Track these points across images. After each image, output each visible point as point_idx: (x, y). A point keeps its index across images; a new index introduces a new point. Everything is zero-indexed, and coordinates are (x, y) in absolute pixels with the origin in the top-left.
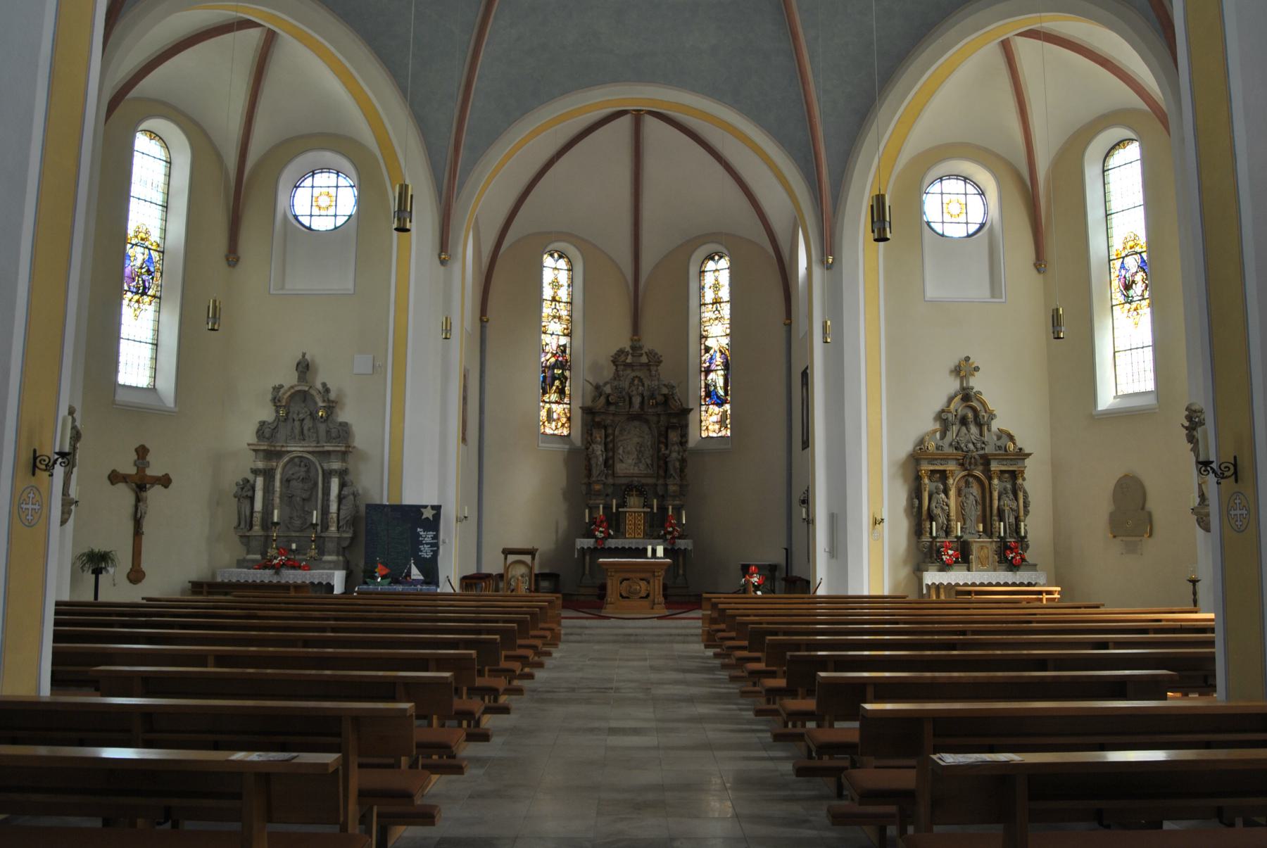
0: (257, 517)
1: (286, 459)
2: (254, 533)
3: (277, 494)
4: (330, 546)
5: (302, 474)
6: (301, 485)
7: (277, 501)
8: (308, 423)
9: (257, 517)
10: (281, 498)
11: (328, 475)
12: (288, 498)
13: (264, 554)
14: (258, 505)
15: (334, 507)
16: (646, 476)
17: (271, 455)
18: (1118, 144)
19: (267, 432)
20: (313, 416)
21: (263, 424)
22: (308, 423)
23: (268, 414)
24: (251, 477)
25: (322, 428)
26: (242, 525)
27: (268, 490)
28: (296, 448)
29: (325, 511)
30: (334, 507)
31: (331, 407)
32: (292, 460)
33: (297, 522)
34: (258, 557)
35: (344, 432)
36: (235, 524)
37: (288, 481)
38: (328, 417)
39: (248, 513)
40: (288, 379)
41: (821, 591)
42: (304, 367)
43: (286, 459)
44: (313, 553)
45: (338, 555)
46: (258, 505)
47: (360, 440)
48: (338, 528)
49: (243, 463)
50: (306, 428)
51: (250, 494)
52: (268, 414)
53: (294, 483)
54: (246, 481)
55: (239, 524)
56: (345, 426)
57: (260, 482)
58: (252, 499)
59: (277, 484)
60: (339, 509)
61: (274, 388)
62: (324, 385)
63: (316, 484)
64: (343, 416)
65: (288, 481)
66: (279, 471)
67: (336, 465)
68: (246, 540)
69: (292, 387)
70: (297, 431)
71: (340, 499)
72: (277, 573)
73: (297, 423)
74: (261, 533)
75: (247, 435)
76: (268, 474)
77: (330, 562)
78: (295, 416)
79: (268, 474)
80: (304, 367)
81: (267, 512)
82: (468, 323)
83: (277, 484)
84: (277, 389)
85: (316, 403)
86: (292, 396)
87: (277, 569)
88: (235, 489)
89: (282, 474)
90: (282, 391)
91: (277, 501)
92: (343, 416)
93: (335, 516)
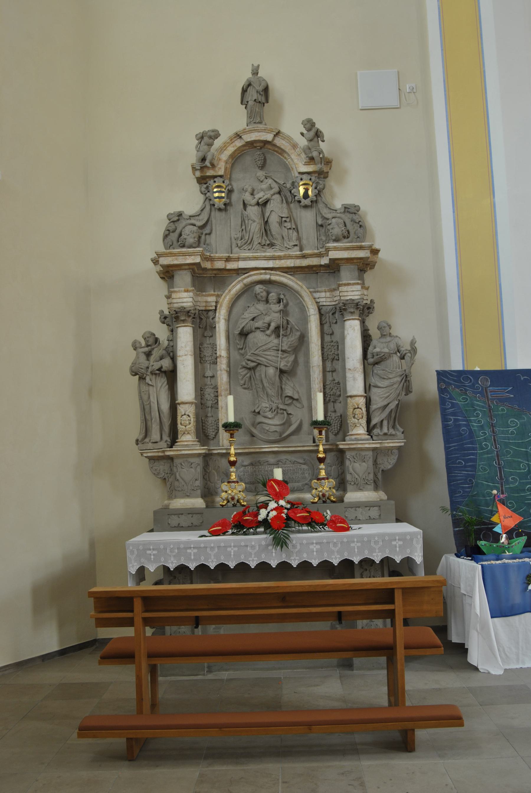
0: (187, 415)
1: (236, 286)
2: (173, 448)
3: (223, 364)
4: (358, 468)
5: (274, 318)
7: (223, 378)
8: (277, 209)
9: (187, 415)
11: (332, 317)
12: (248, 372)
13: (208, 493)
14: (186, 389)
15: (355, 385)
16: (194, 441)
17: (205, 278)
18: (229, 354)
19: (189, 234)
20: (287, 194)
21: (177, 218)
23: (188, 199)
24: (162, 333)
25: (307, 219)
26: (155, 435)
27: (203, 356)
28: (256, 261)
29: (334, 393)
30: (355, 385)
31: (322, 170)
32: (248, 288)
33: (274, 423)
34: (199, 503)
35: (353, 223)
36: (136, 432)
37: (244, 334)
38: (318, 194)
39: (165, 406)
42: (257, 96)
43: (236, 286)
44: (327, 487)
45: (376, 488)
46: (186, 389)
47: (387, 235)
48: (369, 430)
49: (144, 307)
50: (274, 220)
51: (166, 363)
52: (188, 199)
54: (153, 341)
55: (147, 432)
57: (185, 335)
58: (171, 376)
59: (221, 341)
60: (367, 388)
61: (201, 137)
62: (309, 125)
65: (244, 334)
66: (222, 315)
67: (352, 292)
68: (164, 466)
69: (238, 136)
70: (255, 227)
71: (370, 361)
72: (280, 542)
73: (253, 211)
75: (146, 244)
76: (202, 322)
77: (368, 505)
78: (247, 197)
79: (202, 322)
80: (257, 96)
81: (206, 403)
83: (221, 341)
84: (207, 138)
85: (287, 169)
86: (236, 158)
87: (278, 529)
88: (130, 356)
90: (218, 143)
91: (223, 378)
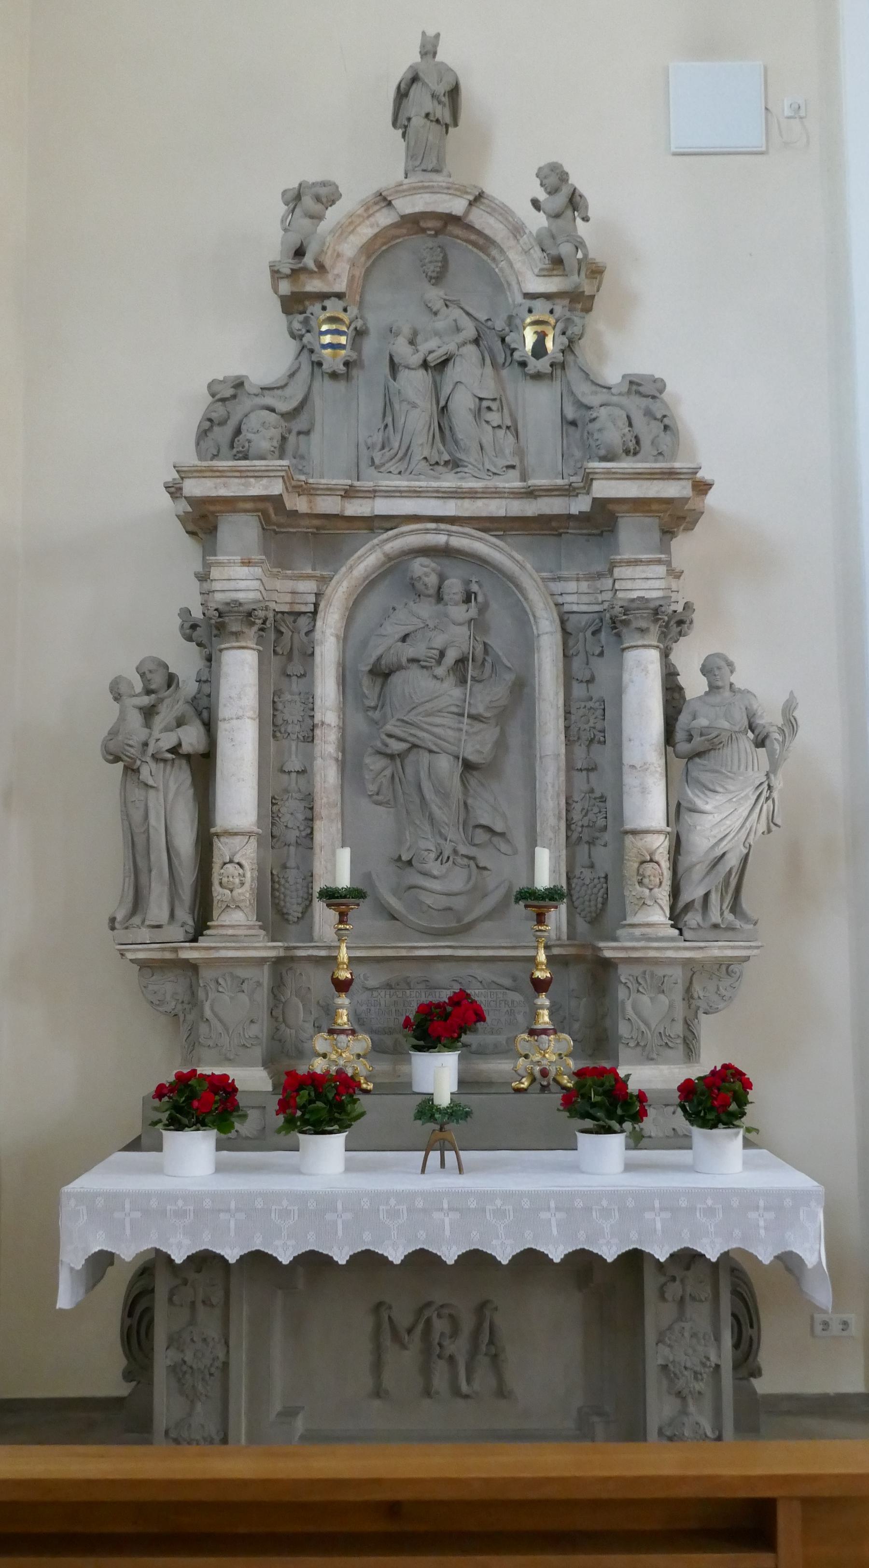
0: (240, 864)
1: (366, 559)
5: (456, 638)
6: (450, 692)
7: (327, 776)
8: (470, 377)
9: (240, 864)
10: (349, 766)
12: (387, 760)
14: (239, 799)
21: (230, 392)
22: (470, 377)
23: (255, 348)
26: (158, 908)
27: (284, 723)
28: (415, 497)
31: (580, 284)
32: (394, 567)
36: (111, 897)
37: (382, 673)
39: (185, 841)
40: (367, 164)
41: (549, 975)
43: (366, 559)
50: (462, 405)
51: (191, 738)
52: (255, 348)
53: (413, 684)
56: (644, 389)
57: (241, 671)
58: (203, 766)
62: (554, 178)
63: (522, 690)
64: (622, 351)
65: (382, 673)
69: (384, 200)
70: (418, 419)
73: (414, 383)
74: (265, 948)
76: (284, 638)
78: (401, 348)
79: (284, 638)
81: (287, 828)
82: (329, 604)
86: (378, 251)
89: (344, 639)
90: (334, 215)
91: (327, 776)
92: (622, 351)
93: (660, 845)
